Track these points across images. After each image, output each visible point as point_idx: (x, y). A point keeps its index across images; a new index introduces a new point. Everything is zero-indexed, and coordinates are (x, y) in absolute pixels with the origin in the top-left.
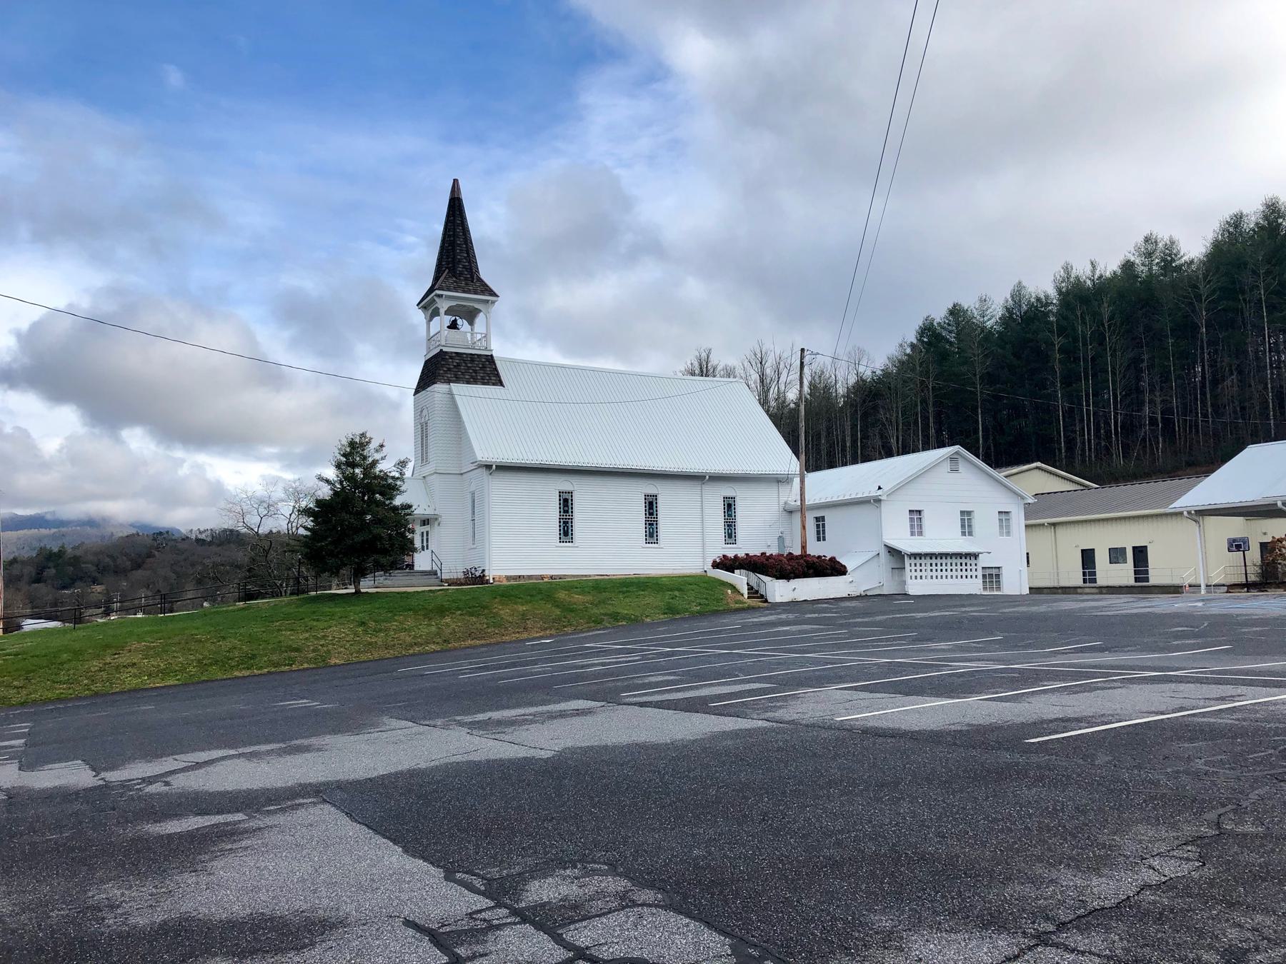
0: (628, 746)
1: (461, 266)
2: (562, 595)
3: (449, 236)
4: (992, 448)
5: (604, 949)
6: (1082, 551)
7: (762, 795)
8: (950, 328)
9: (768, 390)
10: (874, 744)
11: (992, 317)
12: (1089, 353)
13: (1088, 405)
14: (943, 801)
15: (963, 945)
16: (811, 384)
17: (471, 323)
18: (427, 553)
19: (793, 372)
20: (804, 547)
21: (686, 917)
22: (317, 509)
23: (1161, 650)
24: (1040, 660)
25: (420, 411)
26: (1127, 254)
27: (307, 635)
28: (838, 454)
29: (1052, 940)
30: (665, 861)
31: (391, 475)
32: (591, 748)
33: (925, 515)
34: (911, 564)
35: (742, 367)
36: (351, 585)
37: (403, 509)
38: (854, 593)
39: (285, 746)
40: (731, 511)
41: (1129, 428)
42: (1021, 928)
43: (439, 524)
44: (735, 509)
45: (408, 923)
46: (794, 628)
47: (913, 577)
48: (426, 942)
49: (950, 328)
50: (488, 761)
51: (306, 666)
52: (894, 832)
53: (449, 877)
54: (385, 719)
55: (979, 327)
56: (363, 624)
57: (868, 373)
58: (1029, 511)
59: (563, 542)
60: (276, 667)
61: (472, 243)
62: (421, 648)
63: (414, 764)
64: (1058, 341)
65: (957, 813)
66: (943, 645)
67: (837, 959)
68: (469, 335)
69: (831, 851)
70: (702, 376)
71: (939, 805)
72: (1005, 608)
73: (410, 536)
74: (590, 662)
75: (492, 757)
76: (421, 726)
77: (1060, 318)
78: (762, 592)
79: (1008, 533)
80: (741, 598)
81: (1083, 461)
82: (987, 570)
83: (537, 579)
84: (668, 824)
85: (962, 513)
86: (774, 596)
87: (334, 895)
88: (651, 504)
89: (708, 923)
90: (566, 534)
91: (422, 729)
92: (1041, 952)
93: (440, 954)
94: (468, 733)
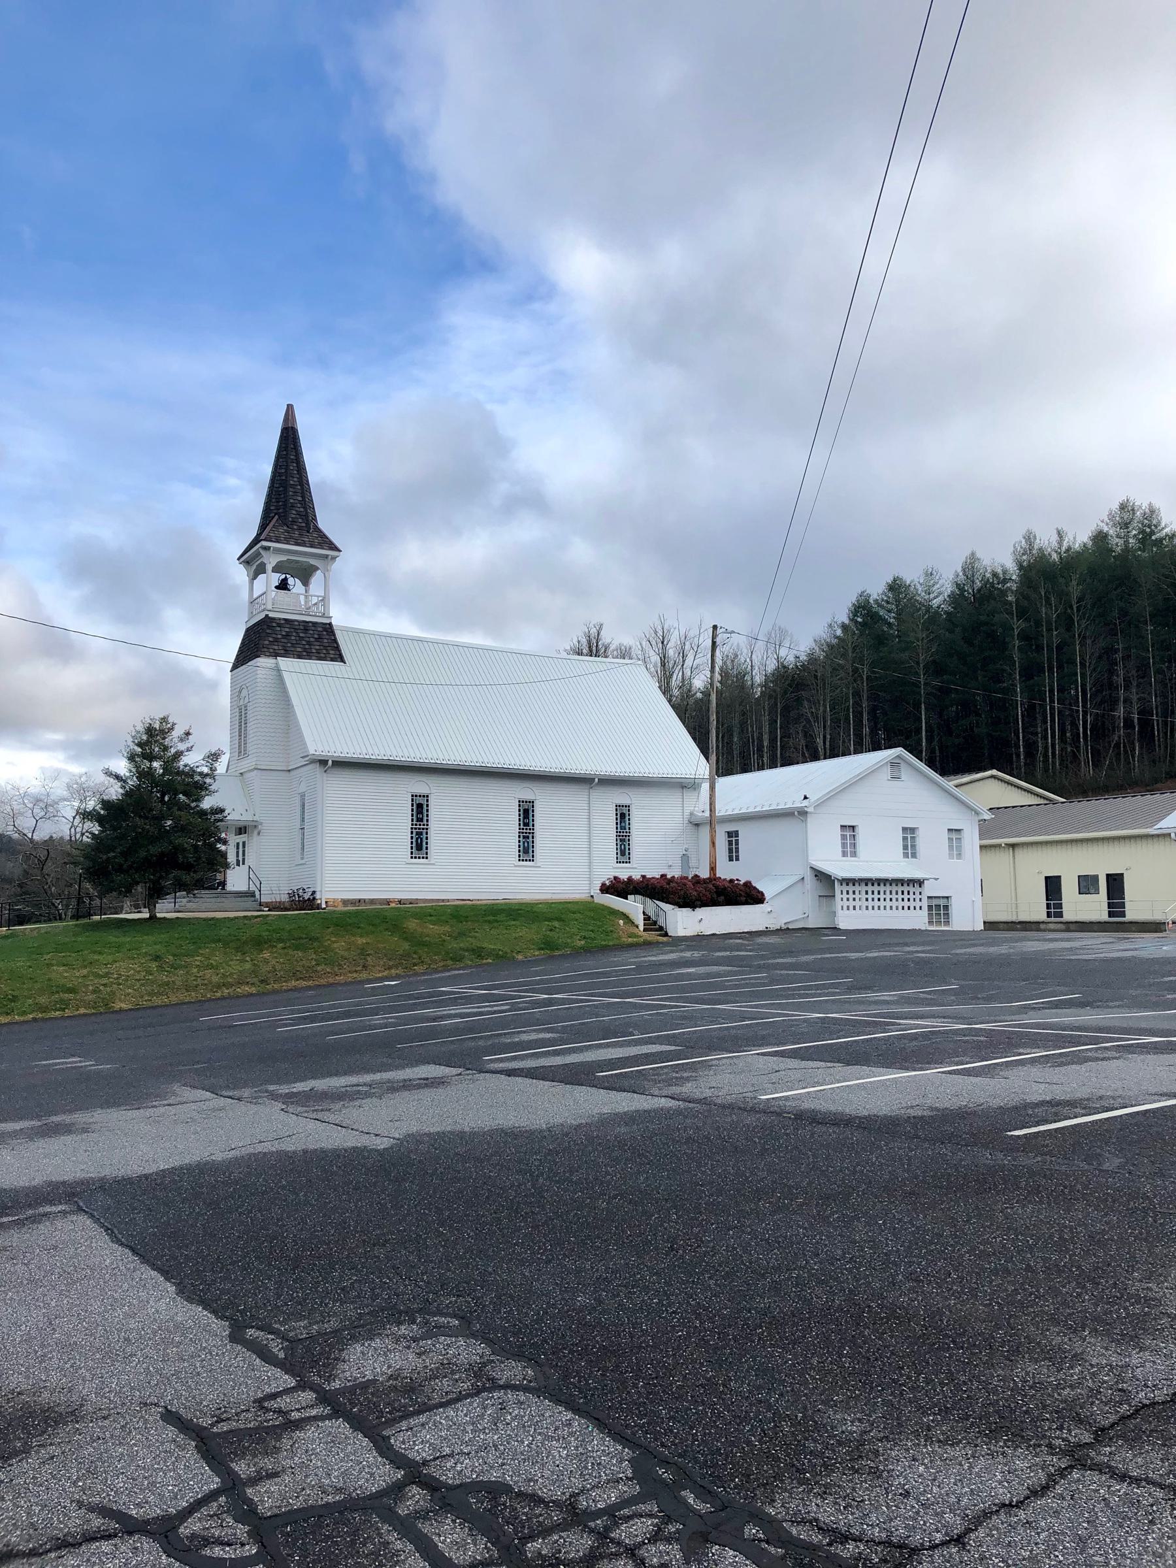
0: (492, 1133)
1: (294, 512)
2: (412, 925)
3: (280, 475)
4: (937, 752)
5: (448, 1465)
6: (1047, 878)
7: (668, 1210)
8: (889, 606)
9: (671, 676)
10: (812, 1136)
11: (940, 594)
12: (1055, 641)
13: (1052, 701)
14: (911, 1222)
15: (966, 1467)
16: (721, 669)
17: (306, 583)
18: (243, 869)
19: (701, 655)
20: (713, 869)
21: (567, 1409)
22: (102, 812)
23: (1155, 1006)
24: (1008, 1018)
25: (238, 691)
26: (1101, 524)
27: (85, 972)
28: (754, 754)
29: (1092, 1459)
30: (539, 1314)
31: (199, 770)
32: (441, 1135)
33: (861, 833)
34: (842, 891)
35: (640, 647)
36: (145, 907)
37: (213, 814)
38: (774, 926)
39: (40, 1123)
40: (625, 822)
41: (1101, 731)
42: (1044, 1436)
43: (259, 834)
44: (629, 819)
45: (171, 1417)
46: (702, 970)
47: (845, 908)
48: (190, 1453)
49: (889, 606)
50: (305, 1152)
51: (82, 1011)
52: (850, 1271)
53: (236, 1337)
54: (176, 1087)
55: (924, 606)
56: (157, 958)
57: (791, 658)
58: (985, 829)
59: (415, 858)
60: (45, 1012)
61: (309, 485)
62: (231, 990)
63: (206, 1154)
64: (1018, 625)
65: (931, 1243)
66: (886, 995)
67: (786, 1490)
68: (302, 598)
69: (766, 1301)
70: (591, 656)
71: (906, 1229)
72: (957, 947)
73: (223, 848)
74: (445, 1012)
75: (311, 1147)
76: (222, 1098)
77: (1021, 598)
78: (661, 922)
79: (959, 856)
80: (635, 930)
81: (1046, 770)
82: (934, 900)
83: (381, 904)
84: (542, 1254)
85: (905, 829)
86: (676, 928)
87: (68, 1366)
88: (526, 812)
89: (597, 1419)
90: (419, 847)
91: (222, 1102)
92: (1079, 1480)
93: (209, 1472)
94: (282, 1110)
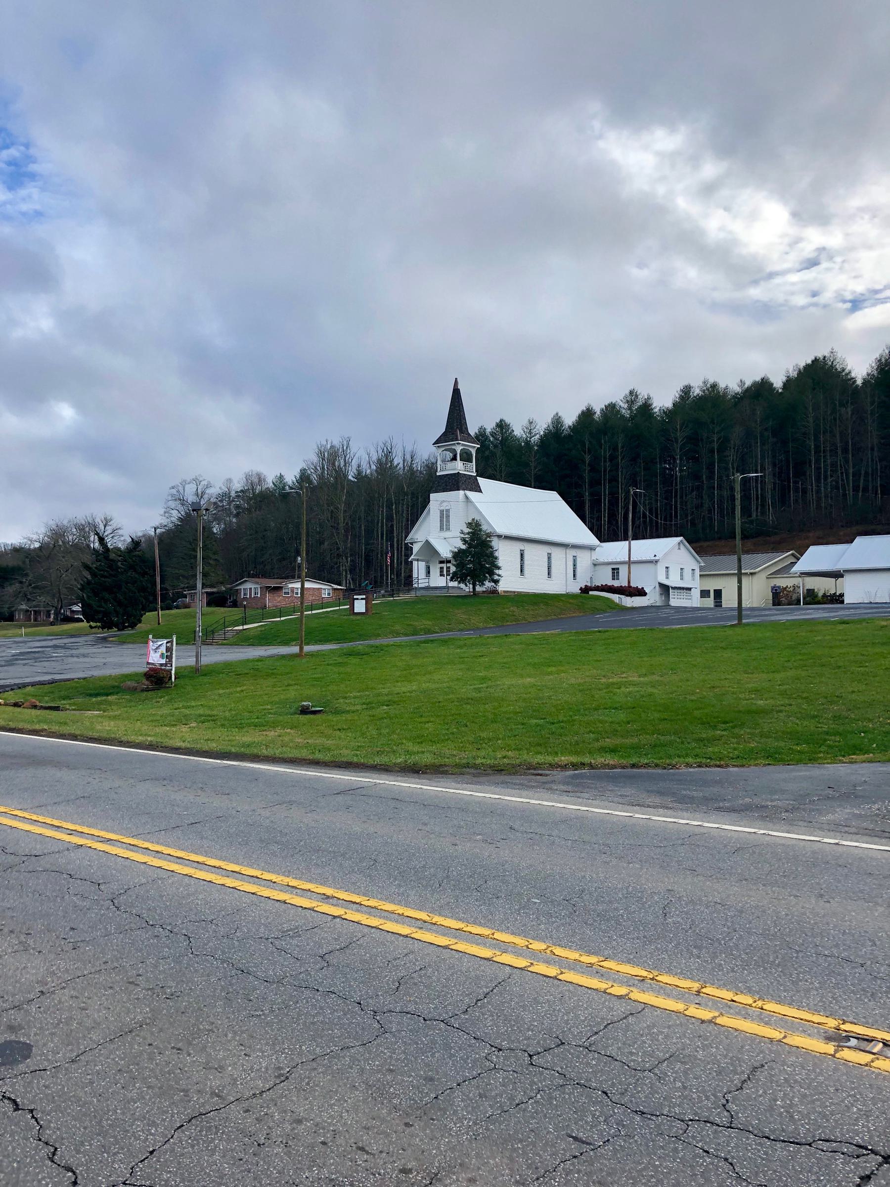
20: (629, 582)
33: (670, 569)
85: (613, 569)
